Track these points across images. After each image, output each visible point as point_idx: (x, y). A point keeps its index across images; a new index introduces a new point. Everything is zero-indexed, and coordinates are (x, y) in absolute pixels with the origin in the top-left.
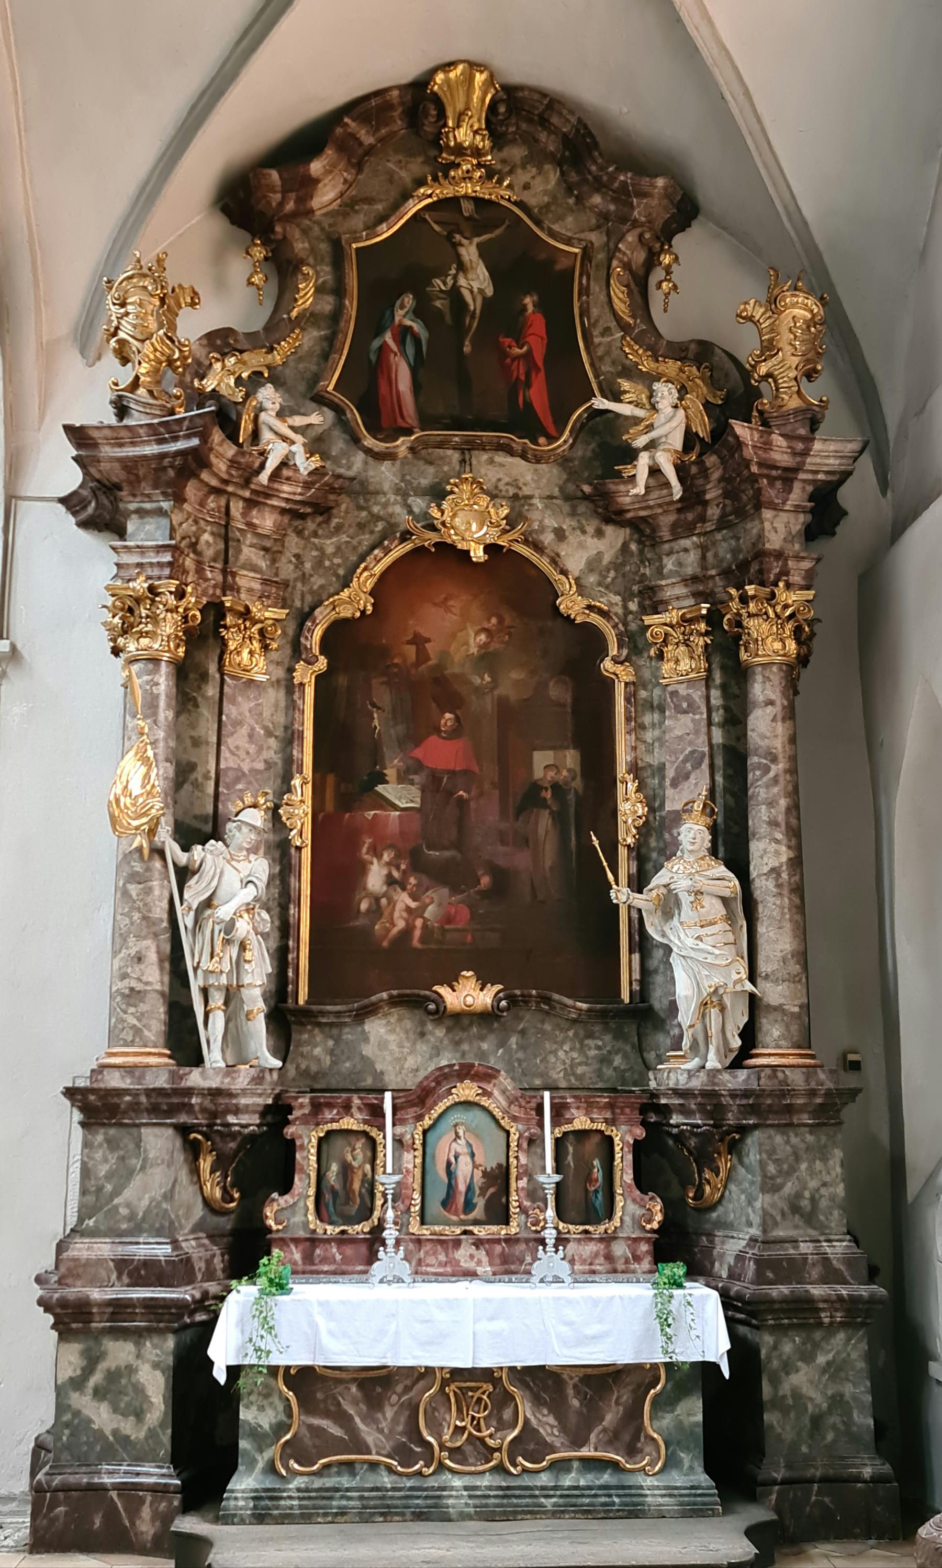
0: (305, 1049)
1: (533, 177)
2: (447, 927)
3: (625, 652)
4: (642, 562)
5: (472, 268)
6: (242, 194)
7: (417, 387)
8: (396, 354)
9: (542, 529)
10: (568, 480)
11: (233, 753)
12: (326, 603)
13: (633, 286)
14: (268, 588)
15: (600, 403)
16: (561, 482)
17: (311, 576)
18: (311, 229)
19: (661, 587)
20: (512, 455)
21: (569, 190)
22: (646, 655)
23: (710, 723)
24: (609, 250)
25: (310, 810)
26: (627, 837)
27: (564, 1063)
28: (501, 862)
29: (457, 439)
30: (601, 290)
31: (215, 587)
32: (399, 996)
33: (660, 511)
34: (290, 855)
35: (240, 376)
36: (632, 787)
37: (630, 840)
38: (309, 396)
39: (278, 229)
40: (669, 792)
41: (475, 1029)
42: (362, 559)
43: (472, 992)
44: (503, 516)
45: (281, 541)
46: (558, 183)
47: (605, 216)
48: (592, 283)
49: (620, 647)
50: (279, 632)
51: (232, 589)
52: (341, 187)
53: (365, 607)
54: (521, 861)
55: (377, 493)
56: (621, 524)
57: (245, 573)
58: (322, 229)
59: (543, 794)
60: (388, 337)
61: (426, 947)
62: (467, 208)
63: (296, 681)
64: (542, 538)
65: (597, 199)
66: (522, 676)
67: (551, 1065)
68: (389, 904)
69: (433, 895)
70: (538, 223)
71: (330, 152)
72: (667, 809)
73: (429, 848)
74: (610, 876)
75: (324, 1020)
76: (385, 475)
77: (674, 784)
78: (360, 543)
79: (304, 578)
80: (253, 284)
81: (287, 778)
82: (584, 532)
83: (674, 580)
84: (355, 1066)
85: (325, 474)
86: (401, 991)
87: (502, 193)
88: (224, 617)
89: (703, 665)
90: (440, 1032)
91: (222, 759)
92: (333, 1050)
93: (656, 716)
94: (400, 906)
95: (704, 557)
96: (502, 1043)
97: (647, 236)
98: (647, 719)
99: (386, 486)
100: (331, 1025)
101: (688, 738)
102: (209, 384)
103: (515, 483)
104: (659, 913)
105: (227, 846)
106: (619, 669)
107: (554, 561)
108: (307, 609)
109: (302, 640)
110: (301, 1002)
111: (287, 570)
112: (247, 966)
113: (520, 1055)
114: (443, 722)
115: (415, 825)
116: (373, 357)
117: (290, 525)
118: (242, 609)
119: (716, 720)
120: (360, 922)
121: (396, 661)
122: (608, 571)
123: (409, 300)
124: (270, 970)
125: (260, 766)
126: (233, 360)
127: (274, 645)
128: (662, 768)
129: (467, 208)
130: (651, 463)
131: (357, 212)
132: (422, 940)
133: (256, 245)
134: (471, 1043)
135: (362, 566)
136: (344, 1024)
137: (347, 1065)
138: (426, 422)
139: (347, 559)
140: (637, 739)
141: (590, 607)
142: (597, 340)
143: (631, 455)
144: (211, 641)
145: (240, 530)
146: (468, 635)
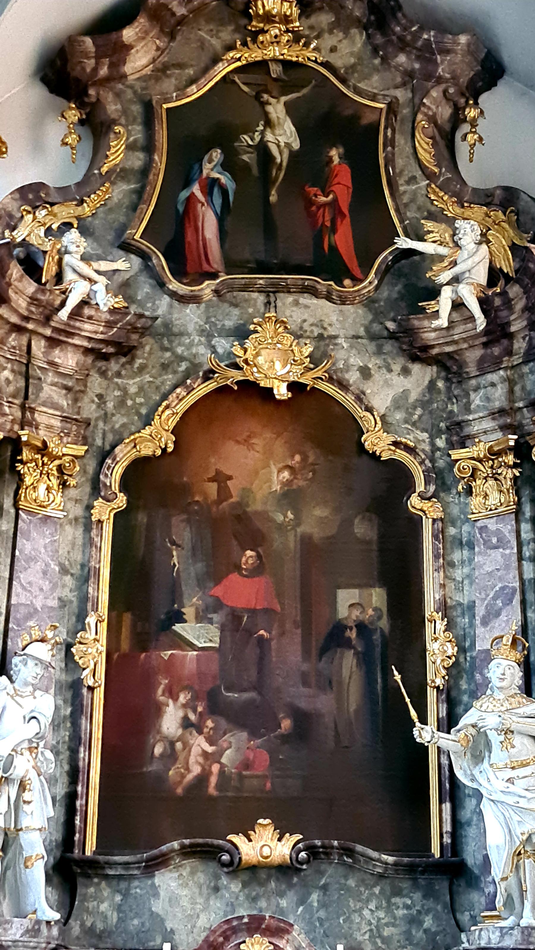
0: (92, 905)
1: (340, 41)
2: (244, 773)
3: (432, 488)
4: (450, 399)
5: (279, 123)
6: (59, 63)
7: (223, 233)
8: (203, 205)
9: (347, 368)
10: (372, 322)
11: (24, 588)
12: (127, 441)
13: (438, 138)
14: (69, 425)
15: (404, 243)
16: (366, 322)
17: (113, 415)
18: (124, 92)
19: (468, 422)
20: (317, 297)
21: (375, 51)
22: (454, 491)
23: (520, 558)
24: (414, 107)
25: (104, 649)
26: (436, 676)
27: (370, 924)
28: (302, 704)
29: (261, 282)
30: (406, 143)
31: (13, 421)
32: (192, 846)
33: (465, 346)
34: (82, 695)
35: (50, 227)
36: (441, 625)
37: (439, 682)
38: (117, 245)
39: (92, 92)
40: (480, 631)
41: (273, 884)
42: (165, 397)
43: (269, 843)
44: (306, 355)
45: (84, 381)
46: (365, 44)
47: (410, 74)
48: (397, 136)
49: (427, 483)
50: (78, 468)
51: (30, 425)
52: (153, 53)
53: (166, 445)
54: (324, 703)
55: (181, 334)
56: (427, 361)
57: (45, 409)
58: (135, 92)
59: (348, 633)
60: (196, 189)
61: (222, 795)
62: (275, 70)
63: (94, 519)
64: (347, 376)
65: (402, 58)
66: (325, 514)
67: (355, 926)
68: (184, 749)
69: (232, 740)
70: (343, 81)
71: (142, 20)
72: (478, 648)
73: (228, 689)
74: (413, 714)
75: (111, 872)
76: (190, 317)
77: (485, 622)
78: (163, 383)
79: (106, 417)
80: (66, 144)
81: (81, 617)
82: (390, 371)
83: (481, 415)
84: (143, 924)
85: (128, 314)
86: (193, 841)
87: (309, 55)
88: (20, 453)
89: (513, 498)
90: (235, 887)
91: (13, 594)
92: (120, 906)
93: (466, 552)
94: (195, 751)
95: (511, 391)
96: (302, 901)
97: (451, 91)
98: (457, 556)
99: (191, 328)
100: (120, 877)
101: (499, 574)
102: (19, 235)
103: (320, 324)
104: (469, 755)
105: (12, 682)
106: (426, 505)
107: (359, 399)
108: (108, 447)
109: (102, 477)
110: (88, 853)
111: (89, 409)
112: (26, 807)
113: (322, 914)
114: (244, 559)
115: (214, 667)
116: (181, 208)
117: (93, 366)
118: (39, 444)
119: (527, 554)
120: (153, 767)
121: (197, 498)
122: (415, 408)
123: (217, 155)
124: (52, 814)
125: (54, 603)
126: (44, 212)
127: (72, 482)
128: (472, 606)
129: (275, 70)
130: (454, 297)
131: (168, 76)
132: (218, 787)
133: (71, 109)
134: (268, 899)
135: (164, 404)
136: (132, 877)
137: (136, 922)
138: (231, 266)
139: (150, 398)
140: (446, 577)
141: (396, 444)
142: (402, 189)
143: (434, 293)
144: (7, 476)
145: (40, 368)
146: (270, 473)
